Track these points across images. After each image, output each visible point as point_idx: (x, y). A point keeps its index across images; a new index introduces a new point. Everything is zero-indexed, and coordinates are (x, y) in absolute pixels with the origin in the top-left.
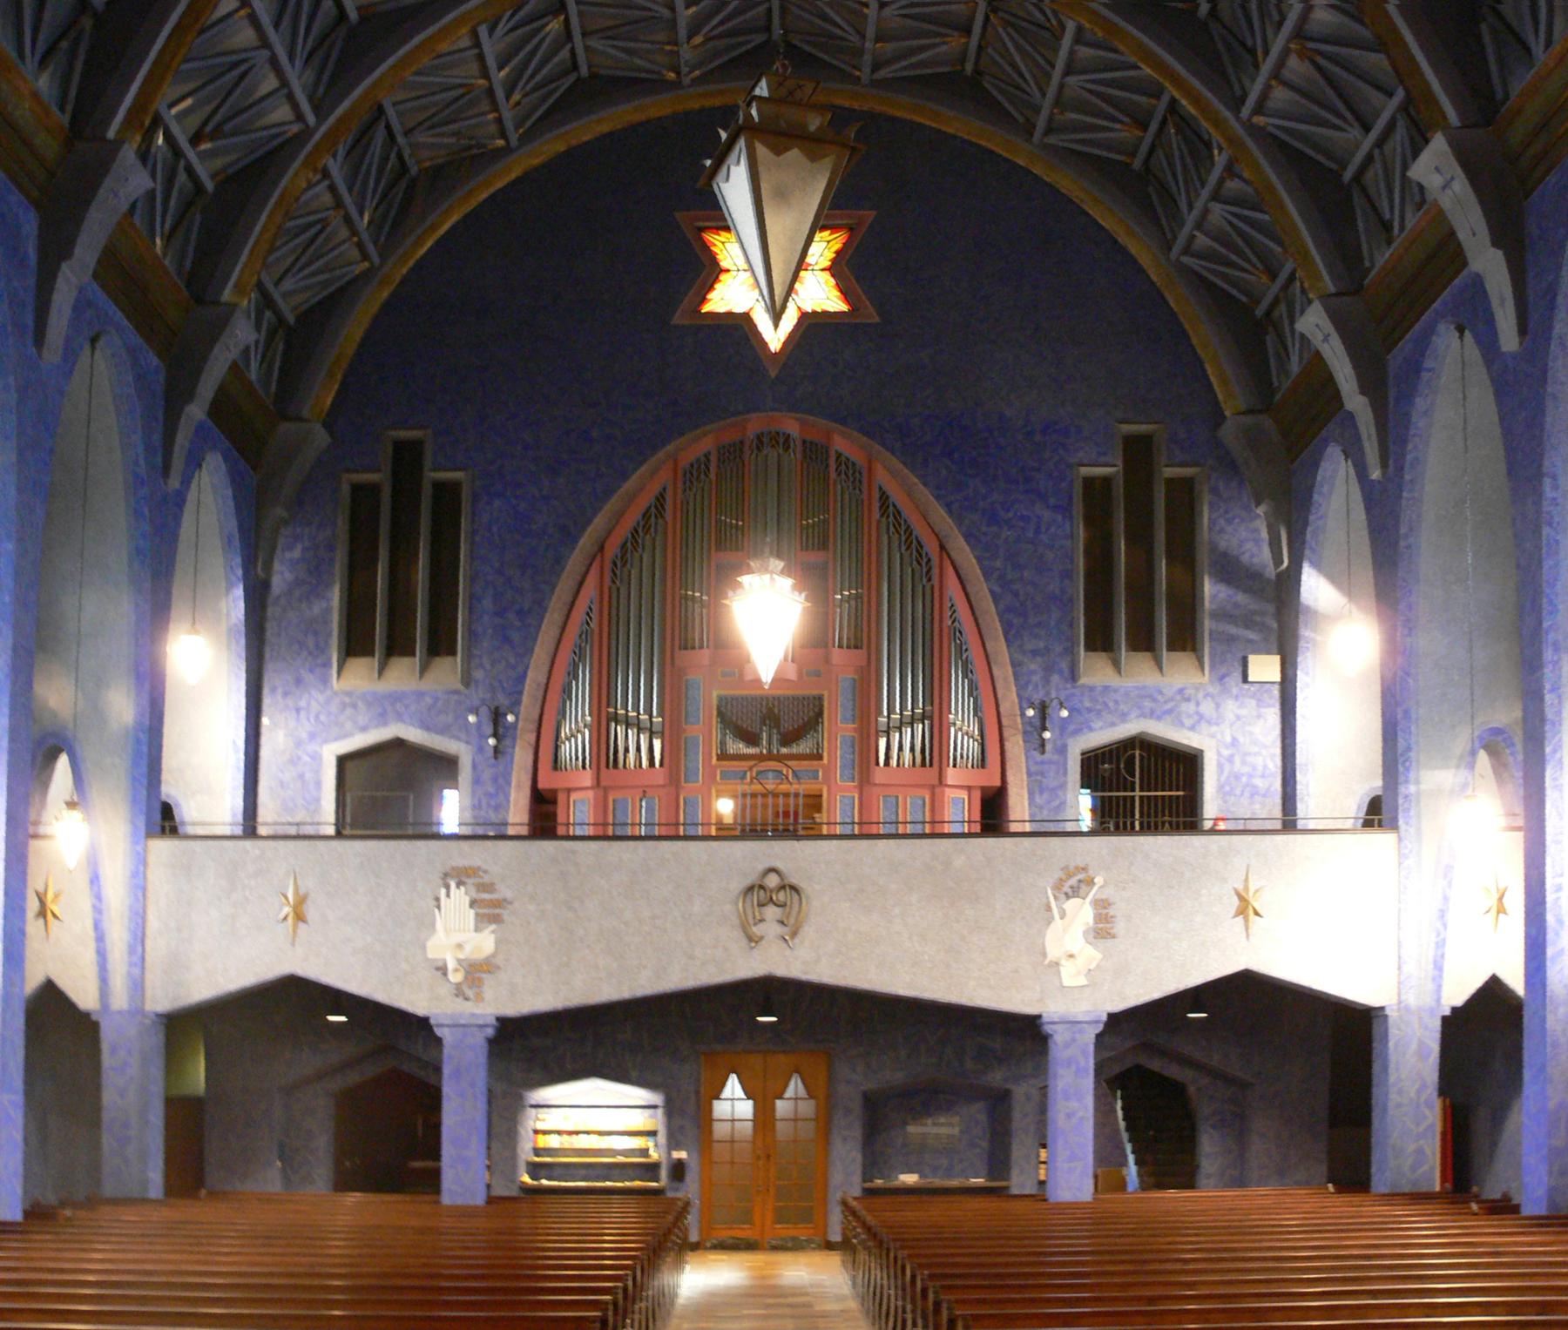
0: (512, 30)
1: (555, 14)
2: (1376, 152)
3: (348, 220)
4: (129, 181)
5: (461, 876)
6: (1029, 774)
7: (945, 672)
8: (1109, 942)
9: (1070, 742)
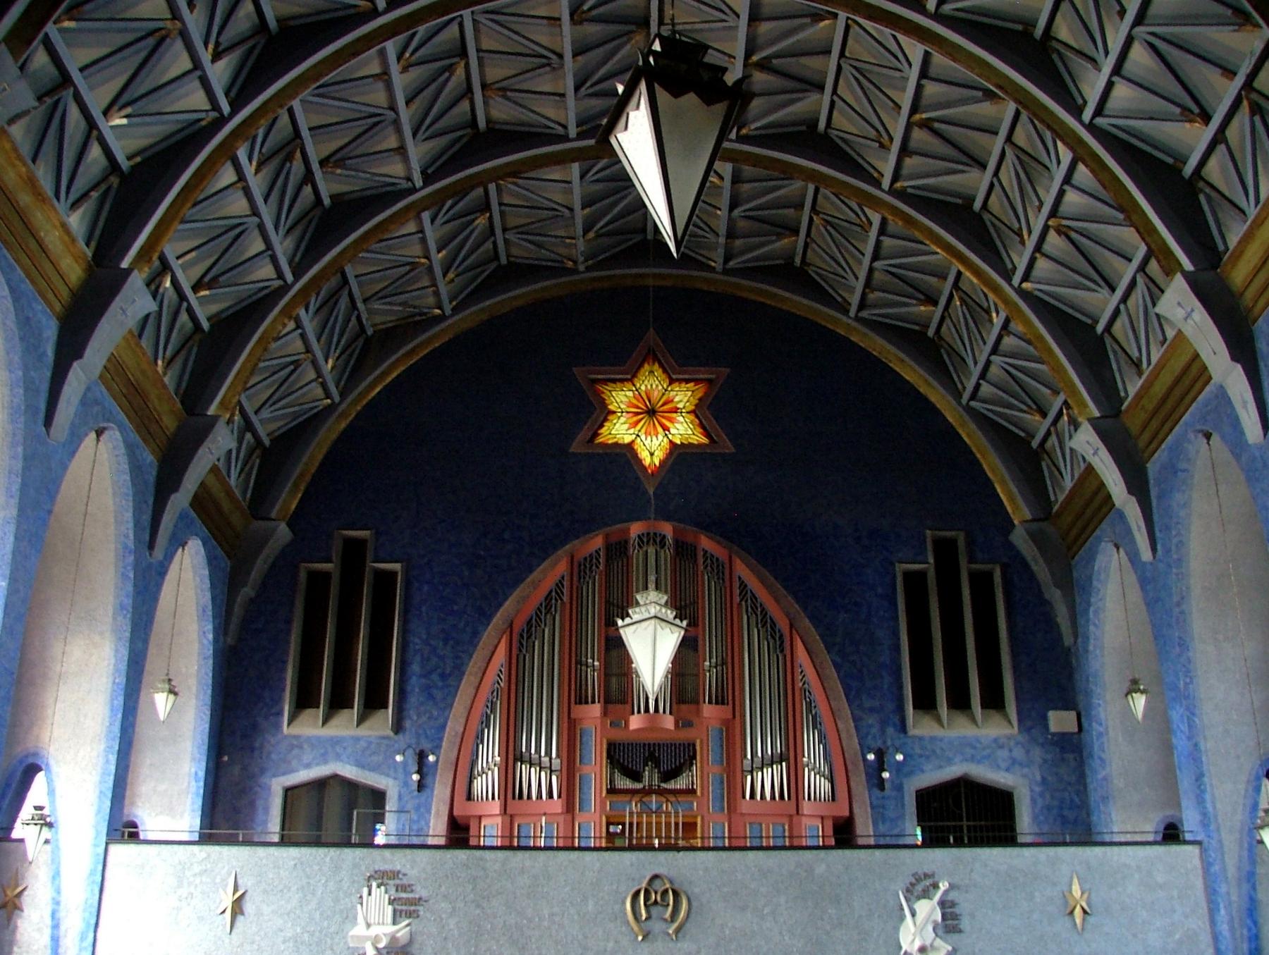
0: (445, 223)
2: (1122, 307)
5: (383, 877)
6: (872, 807)
7: (798, 734)
8: (956, 936)
9: (905, 781)
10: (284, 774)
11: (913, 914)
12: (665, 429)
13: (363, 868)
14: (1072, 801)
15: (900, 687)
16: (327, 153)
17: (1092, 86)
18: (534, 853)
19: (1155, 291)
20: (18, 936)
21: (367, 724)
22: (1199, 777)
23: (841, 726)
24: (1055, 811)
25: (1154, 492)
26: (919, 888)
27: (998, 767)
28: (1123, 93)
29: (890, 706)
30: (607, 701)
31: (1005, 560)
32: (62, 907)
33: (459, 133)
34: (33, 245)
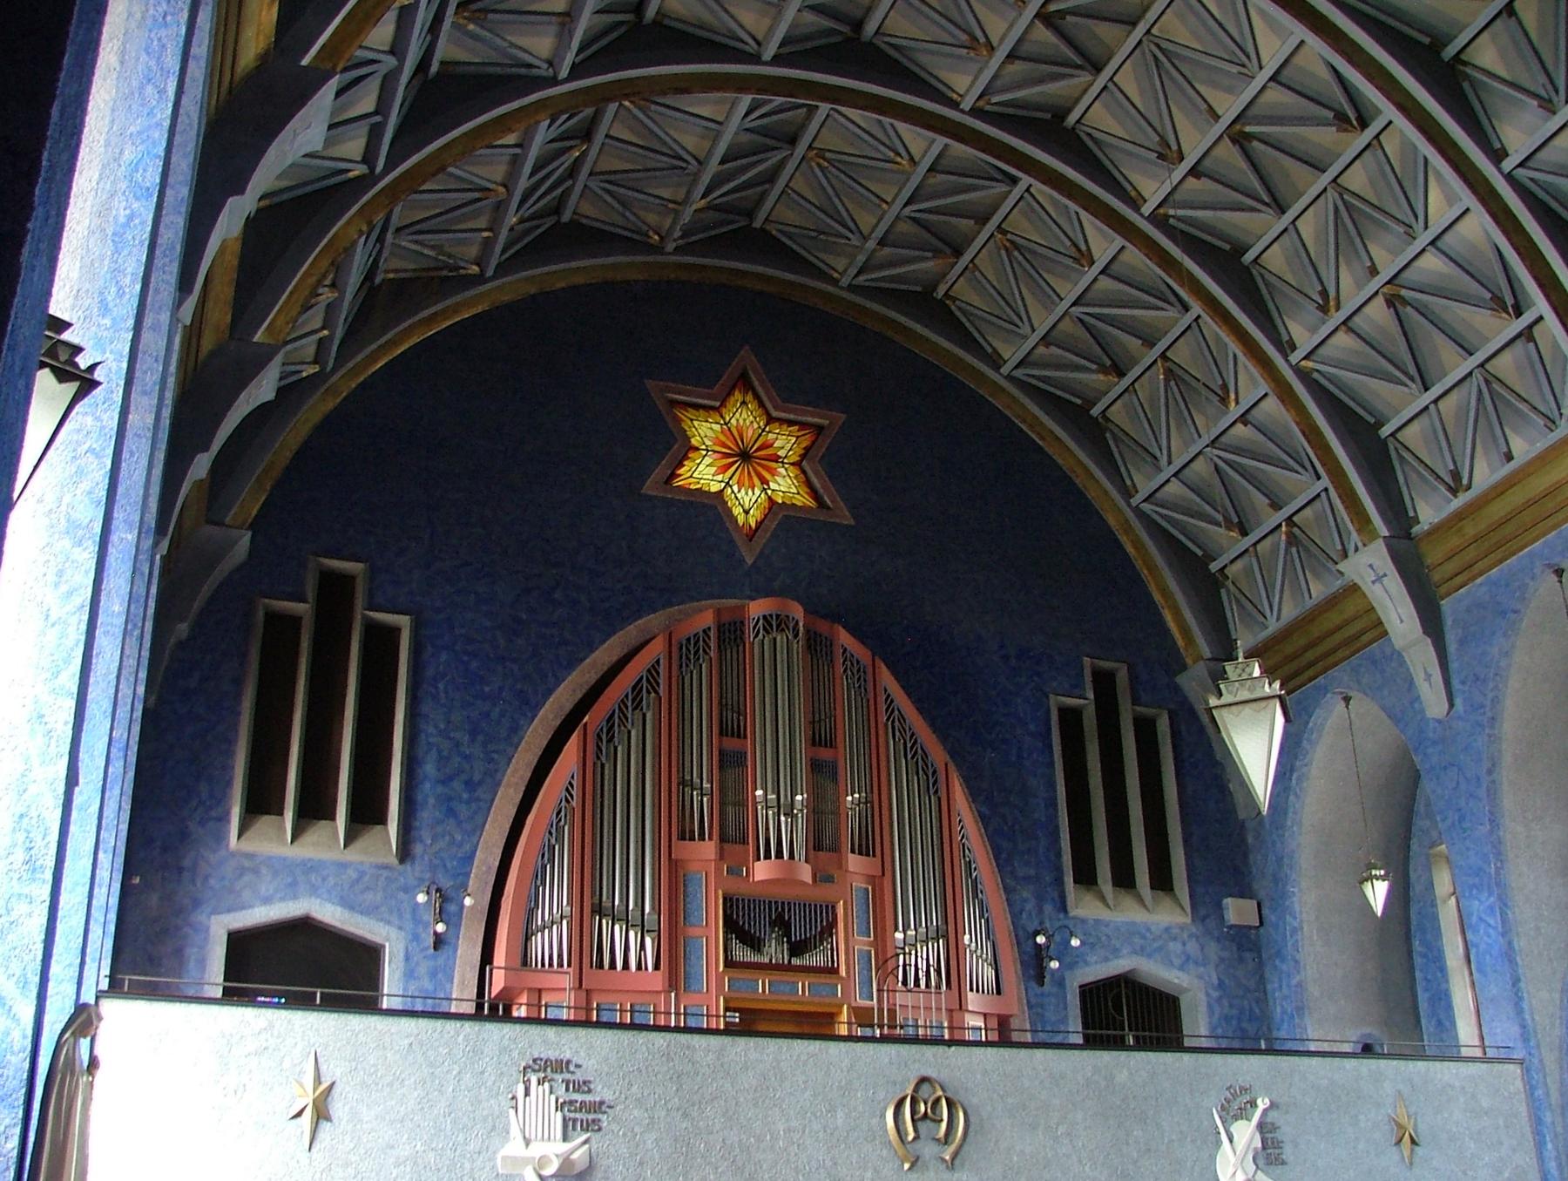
2: (1432, 407)
5: (548, 1068)
6: (1030, 1007)
8: (1279, 1170)
10: (229, 911)
12: (764, 481)
13: (515, 1054)
14: (1251, 1010)
21: (359, 844)
30: (723, 839)
31: (1172, 706)
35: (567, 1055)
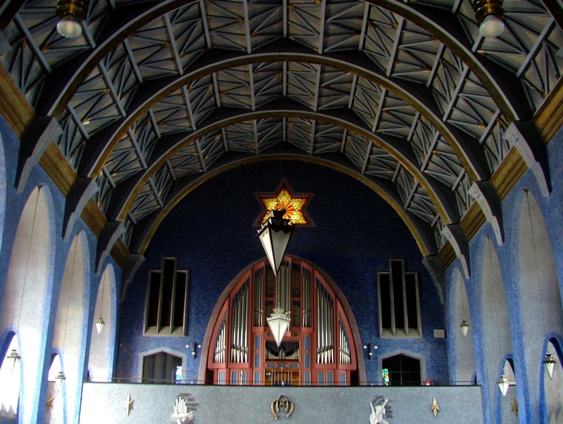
1: (218, 134)
2: (461, 183)
3: (154, 194)
4: (93, 189)
5: (183, 396)
6: (366, 366)
8: (390, 419)
9: (378, 356)
11: (375, 411)
13: (176, 392)
15: (378, 320)
16: (160, 120)
17: (447, 108)
18: (238, 387)
19: (504, 128)
20: (52, 416)
22: (482, 362)
23: (354, 334)
24: (435, 368)
25: (470, 253)
26: (378, 401)
27: (415, 351)
28: (456, 113)
29: (373, 327)
32: (67, 405)
33: (210, 109)
34: (58, 174)
35: (189, 392)
